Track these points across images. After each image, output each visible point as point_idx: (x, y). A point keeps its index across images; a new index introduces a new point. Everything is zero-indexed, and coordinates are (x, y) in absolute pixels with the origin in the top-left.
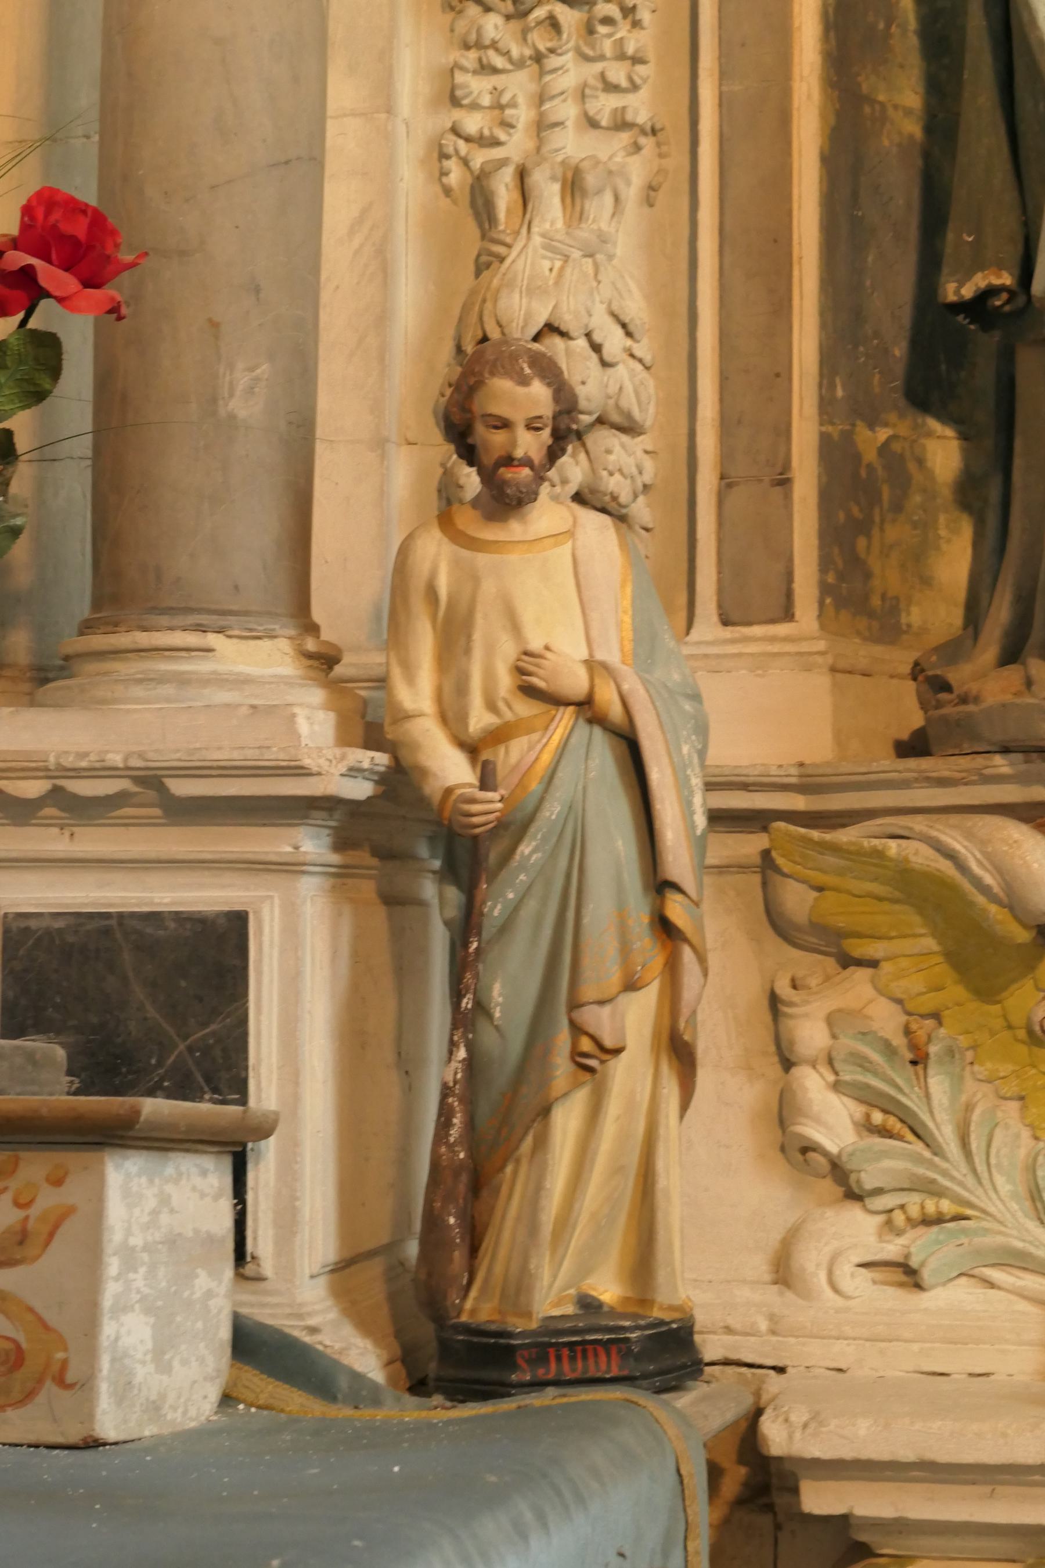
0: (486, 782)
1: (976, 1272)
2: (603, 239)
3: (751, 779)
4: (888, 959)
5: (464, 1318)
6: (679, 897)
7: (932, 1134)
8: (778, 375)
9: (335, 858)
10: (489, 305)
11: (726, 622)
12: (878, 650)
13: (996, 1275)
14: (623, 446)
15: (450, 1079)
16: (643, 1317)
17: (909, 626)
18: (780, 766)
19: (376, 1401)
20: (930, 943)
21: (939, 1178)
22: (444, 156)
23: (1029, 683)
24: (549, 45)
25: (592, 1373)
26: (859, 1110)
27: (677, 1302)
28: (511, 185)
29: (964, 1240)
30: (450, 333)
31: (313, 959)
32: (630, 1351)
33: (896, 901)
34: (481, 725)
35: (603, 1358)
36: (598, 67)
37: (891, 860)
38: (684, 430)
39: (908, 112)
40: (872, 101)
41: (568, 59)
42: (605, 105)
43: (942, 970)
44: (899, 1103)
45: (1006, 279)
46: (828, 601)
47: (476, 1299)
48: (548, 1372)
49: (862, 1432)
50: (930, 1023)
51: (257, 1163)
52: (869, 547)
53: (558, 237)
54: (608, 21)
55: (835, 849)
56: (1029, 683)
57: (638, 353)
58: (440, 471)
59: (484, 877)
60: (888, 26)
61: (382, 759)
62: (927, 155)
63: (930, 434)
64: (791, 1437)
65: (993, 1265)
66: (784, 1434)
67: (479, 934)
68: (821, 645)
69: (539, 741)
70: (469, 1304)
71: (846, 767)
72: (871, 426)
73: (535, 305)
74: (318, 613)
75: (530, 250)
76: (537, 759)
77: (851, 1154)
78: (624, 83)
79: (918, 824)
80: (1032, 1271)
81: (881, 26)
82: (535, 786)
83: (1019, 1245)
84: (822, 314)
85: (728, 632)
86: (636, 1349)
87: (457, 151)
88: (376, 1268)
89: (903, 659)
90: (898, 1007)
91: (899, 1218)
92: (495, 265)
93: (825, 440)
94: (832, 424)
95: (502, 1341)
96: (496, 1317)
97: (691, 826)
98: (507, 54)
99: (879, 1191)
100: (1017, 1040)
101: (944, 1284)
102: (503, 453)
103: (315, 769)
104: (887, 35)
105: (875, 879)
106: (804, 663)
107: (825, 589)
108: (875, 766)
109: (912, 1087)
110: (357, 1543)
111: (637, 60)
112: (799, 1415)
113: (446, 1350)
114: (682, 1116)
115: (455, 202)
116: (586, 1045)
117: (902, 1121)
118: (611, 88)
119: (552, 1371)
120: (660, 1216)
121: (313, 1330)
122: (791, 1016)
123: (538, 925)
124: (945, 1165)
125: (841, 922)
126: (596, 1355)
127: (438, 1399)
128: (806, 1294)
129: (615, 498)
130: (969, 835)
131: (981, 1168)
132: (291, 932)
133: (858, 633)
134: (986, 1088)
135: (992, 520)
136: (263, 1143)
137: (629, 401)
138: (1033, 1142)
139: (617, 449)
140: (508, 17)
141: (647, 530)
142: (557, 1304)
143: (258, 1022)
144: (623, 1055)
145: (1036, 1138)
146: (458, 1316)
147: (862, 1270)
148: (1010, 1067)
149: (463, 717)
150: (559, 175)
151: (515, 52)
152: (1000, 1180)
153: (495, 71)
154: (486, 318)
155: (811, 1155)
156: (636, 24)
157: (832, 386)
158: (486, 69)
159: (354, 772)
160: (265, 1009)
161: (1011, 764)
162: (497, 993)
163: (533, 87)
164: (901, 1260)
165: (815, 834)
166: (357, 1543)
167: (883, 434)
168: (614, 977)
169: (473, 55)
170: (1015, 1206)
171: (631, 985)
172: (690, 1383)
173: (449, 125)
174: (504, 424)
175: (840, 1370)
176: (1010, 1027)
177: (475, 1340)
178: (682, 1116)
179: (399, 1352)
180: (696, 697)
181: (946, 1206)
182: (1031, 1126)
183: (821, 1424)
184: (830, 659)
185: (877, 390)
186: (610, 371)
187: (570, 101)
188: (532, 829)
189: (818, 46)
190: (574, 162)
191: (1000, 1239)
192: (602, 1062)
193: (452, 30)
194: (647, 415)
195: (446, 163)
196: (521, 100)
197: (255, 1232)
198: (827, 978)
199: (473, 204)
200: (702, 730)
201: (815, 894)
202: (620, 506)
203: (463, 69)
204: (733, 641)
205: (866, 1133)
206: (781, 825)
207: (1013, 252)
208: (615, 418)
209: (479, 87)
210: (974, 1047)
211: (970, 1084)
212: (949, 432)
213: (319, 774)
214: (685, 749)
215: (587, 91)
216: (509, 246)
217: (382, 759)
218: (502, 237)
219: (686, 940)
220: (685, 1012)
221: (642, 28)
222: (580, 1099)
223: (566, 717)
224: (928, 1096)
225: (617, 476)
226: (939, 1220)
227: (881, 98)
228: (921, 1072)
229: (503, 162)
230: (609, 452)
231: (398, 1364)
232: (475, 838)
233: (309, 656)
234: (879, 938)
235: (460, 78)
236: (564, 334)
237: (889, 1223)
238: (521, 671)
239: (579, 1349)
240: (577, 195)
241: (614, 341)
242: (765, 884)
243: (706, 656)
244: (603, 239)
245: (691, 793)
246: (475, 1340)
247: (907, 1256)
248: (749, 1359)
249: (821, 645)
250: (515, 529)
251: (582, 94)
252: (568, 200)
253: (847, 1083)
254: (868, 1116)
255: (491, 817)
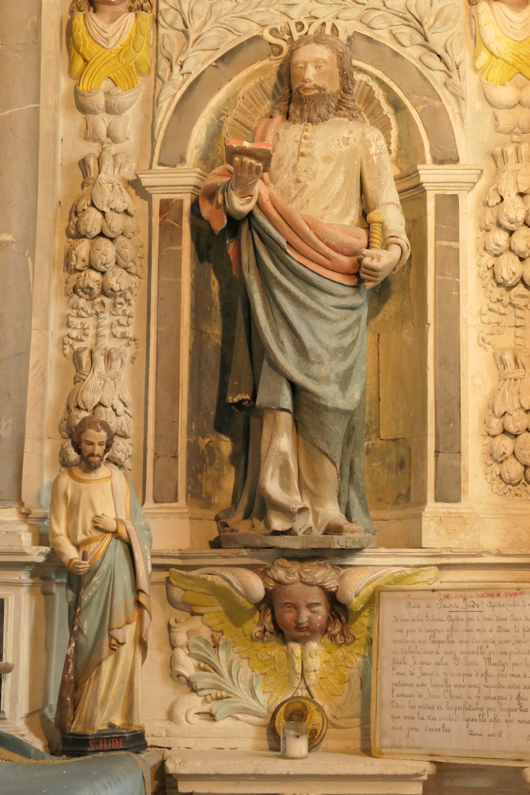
0: (84, 558)
1: (233, 715)
2: (117, 374)
3: (164, 554)
4: (207, 613)
5: (72, 731)
6: (143, 595)
7: (220, 670)
8: (174, 422)
9: (31, 581)
10: (80, 395)
11: (155, 502)
12: (205, 511)
13: (239, 716)
14: (123, 443)
15: (69, 653)
16: (130, 729)
17: (214, 503)
18: (173, 550)
19: (43, 758)
20: (220, 608)
21: (222, 685)
22: (64, 344)
23: (253, 526)
24: (101, 310)
25: (113, 747)
26: (196, 663)
27: (140, 725)
28: (88, 356)
29: (230, 705)
30: (65, 401)
31: (24, 614)
32: (126, 740)
33: (210, 595)
34: (81, 539)
35: (117, 742)
36: (117, 318)
37: (209, 581)
38: (142, 437)
39: (217, 336)
40: (205, 333)
41: (107, 315)
42: (118, 330)
43: (224, 617)
44: (209, 660)
45: (248, 397)
46: (189, 495)
47: (76, 725)
48: (99, 747)
49: (198, 765)
50: (220, 634)
51: (5, 681)
52: (202, 478)
53: (103, 374)
54: (121, 304)
55: (190, 577)
56: (253, 526)
57: (128, 412)
58: (60, 448)
59: (82, 588)
60: (211, 308)
61: (48, 549)
62: (222, 350)
63: (222, 440)
64: (175, 767)
65: (238, 713)
66: (174, 767)
67: (80, 606)
68: (187, 510)
69: (100, 544)
70: (73, 726)
71: (194, 551)
72: (203, 438)
73: (95, 396)
74: (24, 499)
75: (94, 378)
76: (99, 550)
77: (194, 677)
78: (125, 324)
79: (218, 570)
80: (251, 715)
81: (209, 308)
82: (99, 559)
83: (247, 706)
84: (189, 402)
85: (156, 505)
86: (127, 739)
87: (69, 343)
88: (37, 716)
89: (212, 514)
90: (210, 629)
91: (209, 698)
92: (82, 381)
93: (189, 443)
94: (191, 438)
95: (85, 738)
96: (82, 730)
97: (147, 571)
98: (87, 312)
99: (202, 689)
100: (247, 639)
101: (223, 719)
102: (90, 452)
103: (29, 553)
104: (211, 311)
105: (204, 587)
106: (181, 516)
107: (188, 492)
108: (204, 551)
109: (214, 655)
110: (65, 787)
111: (129, 316)
112: (178, 761)
113: (65, 741)
114: (142, 665)
115: (67, 359)
116: (114, 642)
117: (210, 666)
118: (120, 325)
119: (101, 747)
120: (135, 697)
121: (23, 735)
122: (175, 632)
123: (99, 603)
124: (224, 680)
125: (192, 601)
126: (115, 742)
127: (64, 756)
128: (178, 723)
129: (120, 460)
130: (234, 574)
131: (235, 681)
132: (18, 605)
133: (198, 506)
134: (237, 655)
135: (242, 470)
136: (7, 674)
137: (125, 428)
138: (252, 672)
139: (121, 444)
140: (87, 300)
141: (129, 470)
142: (102, 725)
143: (7, 635)
144: (125, 645)
145: (253, 671)
146: (70, 730)
147: (196, 715)
148: (245, 648)
149: (76, 536)
150: (104, 354)
151: (89, 312)
152: (241, 685)
153: (82, 317)
154: (78, 400)
155: (181, 678)
156: (129, 305)
157: (191, 426)
158: (79, 316)
159: (41, 554)
160: (9, 630)
161: (247, 552)
162: (85, 626)
163: (95, 323)
164: (209, 712)
165: (184, 573)
166: (65, 787)
167: (207, 440)
168: (123, 620)
169: (75, 311)
170: (246, 693)
171: (128, 623)
172: (142, 752)
173: (67, 333)
174: (92, 444)
175: (189, 748)
176: (245, 635)
177: (76, 737)
178: (142, 665)
179: (47, 743)
180: (149, 530)
181: (224, 694)
182: (252, 668)
183: (185, 763)
184: (189, 515)
185: (205, 426)
186: (119, 418)
187: (107, 328)
188: (98, 573)
189: (189, 317)
190: (108, 349)
191: (241, 704)
192: (118, 647)
193: (68, 303)
194: (131, 432)
195: (65, 346)
196: (91, 327)
197: (4, 704)
198: (187, 619)
199: (74, 360)
200: (150, 540)
201: (184, 592)
202: (121, 462)
203: (71, 316)
204: (158, 508)
205: (198, 670)
206: (173, 569)
207: (250, 389)
208: (120, 433)
209: (76, 322)
210: (234, 642)
211: (232, 654)
212: (228, 439)
213: (30, 555)
214: (146, 547)
215: (113, 326)
216: (87, 376)
217: (48, 549)
218: (84, 373)
219: (145, 608)
220: (145, 632)
221: (131, 306)
222: (111, 659)
223: (109, 537)
224: (219, 658)
225: (121, 453)
226: (221, 698)
227: (208, 332)
228: (217, 650)
229: (85, 349)
230: (118, 445)
231: (47, 747)
232: (80, 576)
233: (22, 514)
234: (204, 606)
235: (70, 319)
236: (105, 406)
237: (205, 700)
238: (94, 522)
239: (110, 740)
240: (110, 360)
241: (120, 408)
242: (167, 588)
243: (149, 513)
244: (117, 374)
245: (147, 561)
246: (76, 737)
247: (211, 710)
248: (159, 745)
249: (187, 510)
250: (93, 476)
251: (111, 326)
252: (106, 362)
253: (192, 654)
254: (199, 665)
255: (86, 569)
